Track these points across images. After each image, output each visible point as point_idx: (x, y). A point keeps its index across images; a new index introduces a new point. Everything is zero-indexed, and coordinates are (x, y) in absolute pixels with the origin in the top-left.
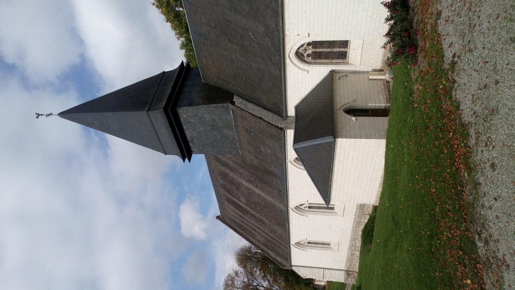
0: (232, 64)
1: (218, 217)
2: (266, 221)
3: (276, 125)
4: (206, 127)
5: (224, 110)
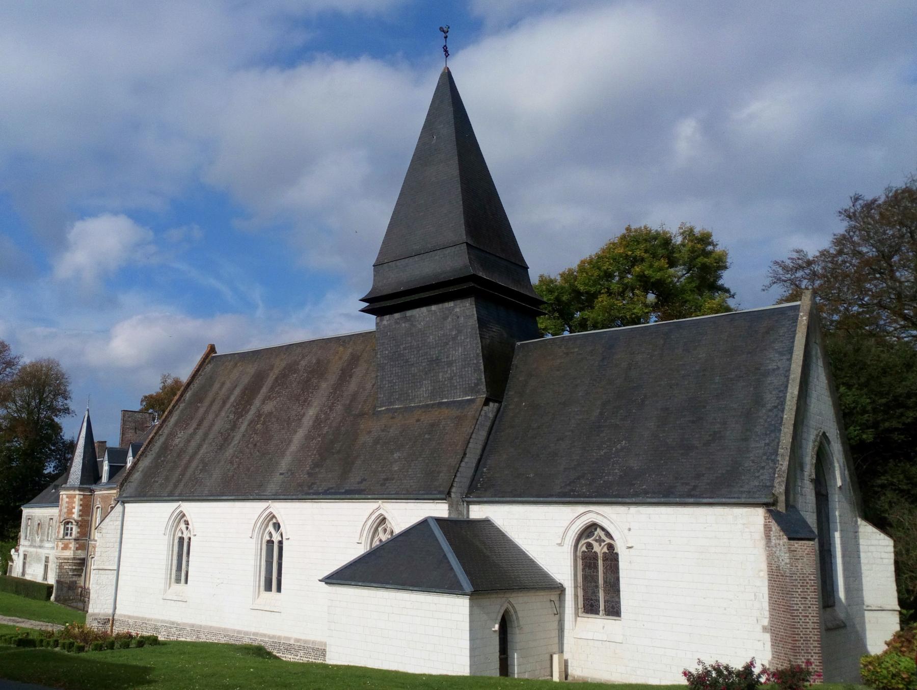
0: (560, 403)
1: (212, 349)
2: (227, 454)
3: (455, 485)
4: (435, 348)
5: (473, 385)
